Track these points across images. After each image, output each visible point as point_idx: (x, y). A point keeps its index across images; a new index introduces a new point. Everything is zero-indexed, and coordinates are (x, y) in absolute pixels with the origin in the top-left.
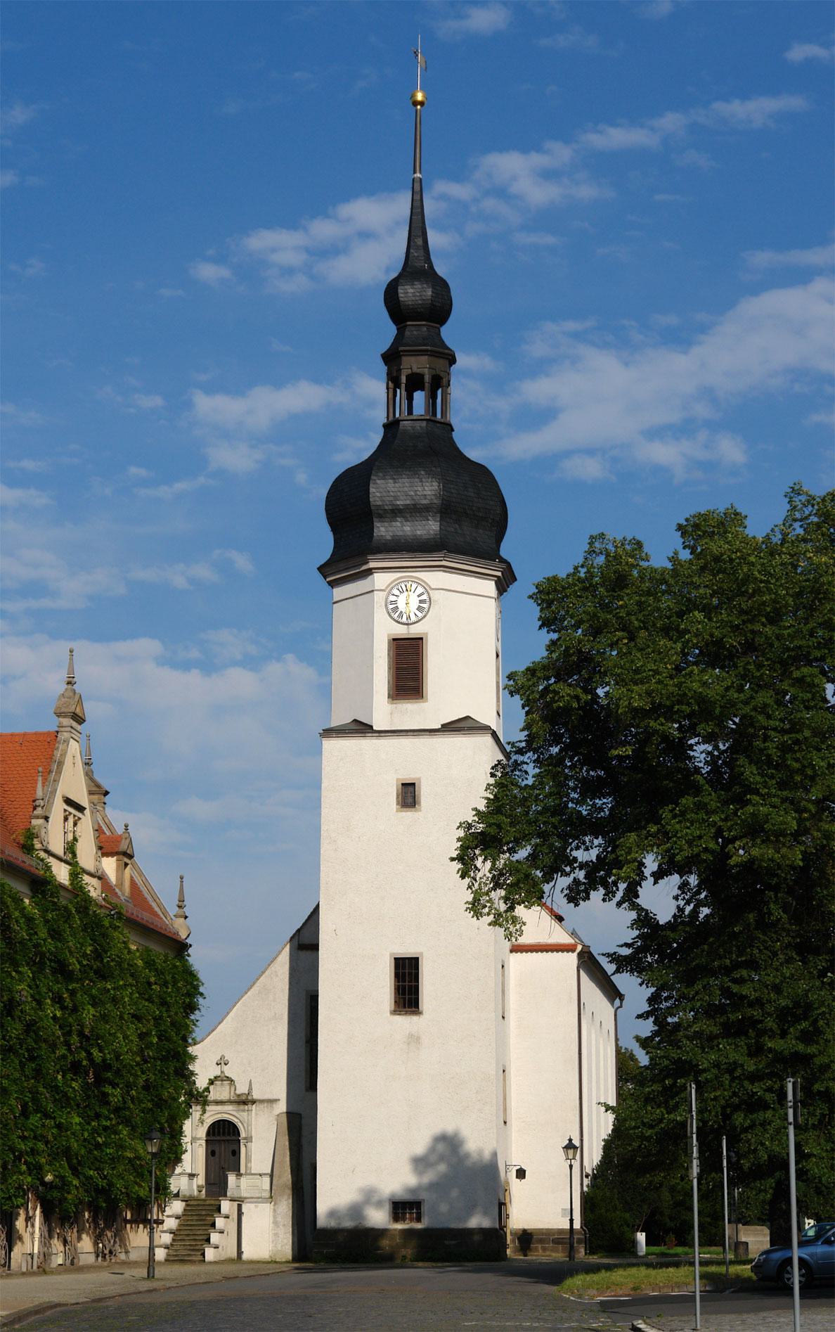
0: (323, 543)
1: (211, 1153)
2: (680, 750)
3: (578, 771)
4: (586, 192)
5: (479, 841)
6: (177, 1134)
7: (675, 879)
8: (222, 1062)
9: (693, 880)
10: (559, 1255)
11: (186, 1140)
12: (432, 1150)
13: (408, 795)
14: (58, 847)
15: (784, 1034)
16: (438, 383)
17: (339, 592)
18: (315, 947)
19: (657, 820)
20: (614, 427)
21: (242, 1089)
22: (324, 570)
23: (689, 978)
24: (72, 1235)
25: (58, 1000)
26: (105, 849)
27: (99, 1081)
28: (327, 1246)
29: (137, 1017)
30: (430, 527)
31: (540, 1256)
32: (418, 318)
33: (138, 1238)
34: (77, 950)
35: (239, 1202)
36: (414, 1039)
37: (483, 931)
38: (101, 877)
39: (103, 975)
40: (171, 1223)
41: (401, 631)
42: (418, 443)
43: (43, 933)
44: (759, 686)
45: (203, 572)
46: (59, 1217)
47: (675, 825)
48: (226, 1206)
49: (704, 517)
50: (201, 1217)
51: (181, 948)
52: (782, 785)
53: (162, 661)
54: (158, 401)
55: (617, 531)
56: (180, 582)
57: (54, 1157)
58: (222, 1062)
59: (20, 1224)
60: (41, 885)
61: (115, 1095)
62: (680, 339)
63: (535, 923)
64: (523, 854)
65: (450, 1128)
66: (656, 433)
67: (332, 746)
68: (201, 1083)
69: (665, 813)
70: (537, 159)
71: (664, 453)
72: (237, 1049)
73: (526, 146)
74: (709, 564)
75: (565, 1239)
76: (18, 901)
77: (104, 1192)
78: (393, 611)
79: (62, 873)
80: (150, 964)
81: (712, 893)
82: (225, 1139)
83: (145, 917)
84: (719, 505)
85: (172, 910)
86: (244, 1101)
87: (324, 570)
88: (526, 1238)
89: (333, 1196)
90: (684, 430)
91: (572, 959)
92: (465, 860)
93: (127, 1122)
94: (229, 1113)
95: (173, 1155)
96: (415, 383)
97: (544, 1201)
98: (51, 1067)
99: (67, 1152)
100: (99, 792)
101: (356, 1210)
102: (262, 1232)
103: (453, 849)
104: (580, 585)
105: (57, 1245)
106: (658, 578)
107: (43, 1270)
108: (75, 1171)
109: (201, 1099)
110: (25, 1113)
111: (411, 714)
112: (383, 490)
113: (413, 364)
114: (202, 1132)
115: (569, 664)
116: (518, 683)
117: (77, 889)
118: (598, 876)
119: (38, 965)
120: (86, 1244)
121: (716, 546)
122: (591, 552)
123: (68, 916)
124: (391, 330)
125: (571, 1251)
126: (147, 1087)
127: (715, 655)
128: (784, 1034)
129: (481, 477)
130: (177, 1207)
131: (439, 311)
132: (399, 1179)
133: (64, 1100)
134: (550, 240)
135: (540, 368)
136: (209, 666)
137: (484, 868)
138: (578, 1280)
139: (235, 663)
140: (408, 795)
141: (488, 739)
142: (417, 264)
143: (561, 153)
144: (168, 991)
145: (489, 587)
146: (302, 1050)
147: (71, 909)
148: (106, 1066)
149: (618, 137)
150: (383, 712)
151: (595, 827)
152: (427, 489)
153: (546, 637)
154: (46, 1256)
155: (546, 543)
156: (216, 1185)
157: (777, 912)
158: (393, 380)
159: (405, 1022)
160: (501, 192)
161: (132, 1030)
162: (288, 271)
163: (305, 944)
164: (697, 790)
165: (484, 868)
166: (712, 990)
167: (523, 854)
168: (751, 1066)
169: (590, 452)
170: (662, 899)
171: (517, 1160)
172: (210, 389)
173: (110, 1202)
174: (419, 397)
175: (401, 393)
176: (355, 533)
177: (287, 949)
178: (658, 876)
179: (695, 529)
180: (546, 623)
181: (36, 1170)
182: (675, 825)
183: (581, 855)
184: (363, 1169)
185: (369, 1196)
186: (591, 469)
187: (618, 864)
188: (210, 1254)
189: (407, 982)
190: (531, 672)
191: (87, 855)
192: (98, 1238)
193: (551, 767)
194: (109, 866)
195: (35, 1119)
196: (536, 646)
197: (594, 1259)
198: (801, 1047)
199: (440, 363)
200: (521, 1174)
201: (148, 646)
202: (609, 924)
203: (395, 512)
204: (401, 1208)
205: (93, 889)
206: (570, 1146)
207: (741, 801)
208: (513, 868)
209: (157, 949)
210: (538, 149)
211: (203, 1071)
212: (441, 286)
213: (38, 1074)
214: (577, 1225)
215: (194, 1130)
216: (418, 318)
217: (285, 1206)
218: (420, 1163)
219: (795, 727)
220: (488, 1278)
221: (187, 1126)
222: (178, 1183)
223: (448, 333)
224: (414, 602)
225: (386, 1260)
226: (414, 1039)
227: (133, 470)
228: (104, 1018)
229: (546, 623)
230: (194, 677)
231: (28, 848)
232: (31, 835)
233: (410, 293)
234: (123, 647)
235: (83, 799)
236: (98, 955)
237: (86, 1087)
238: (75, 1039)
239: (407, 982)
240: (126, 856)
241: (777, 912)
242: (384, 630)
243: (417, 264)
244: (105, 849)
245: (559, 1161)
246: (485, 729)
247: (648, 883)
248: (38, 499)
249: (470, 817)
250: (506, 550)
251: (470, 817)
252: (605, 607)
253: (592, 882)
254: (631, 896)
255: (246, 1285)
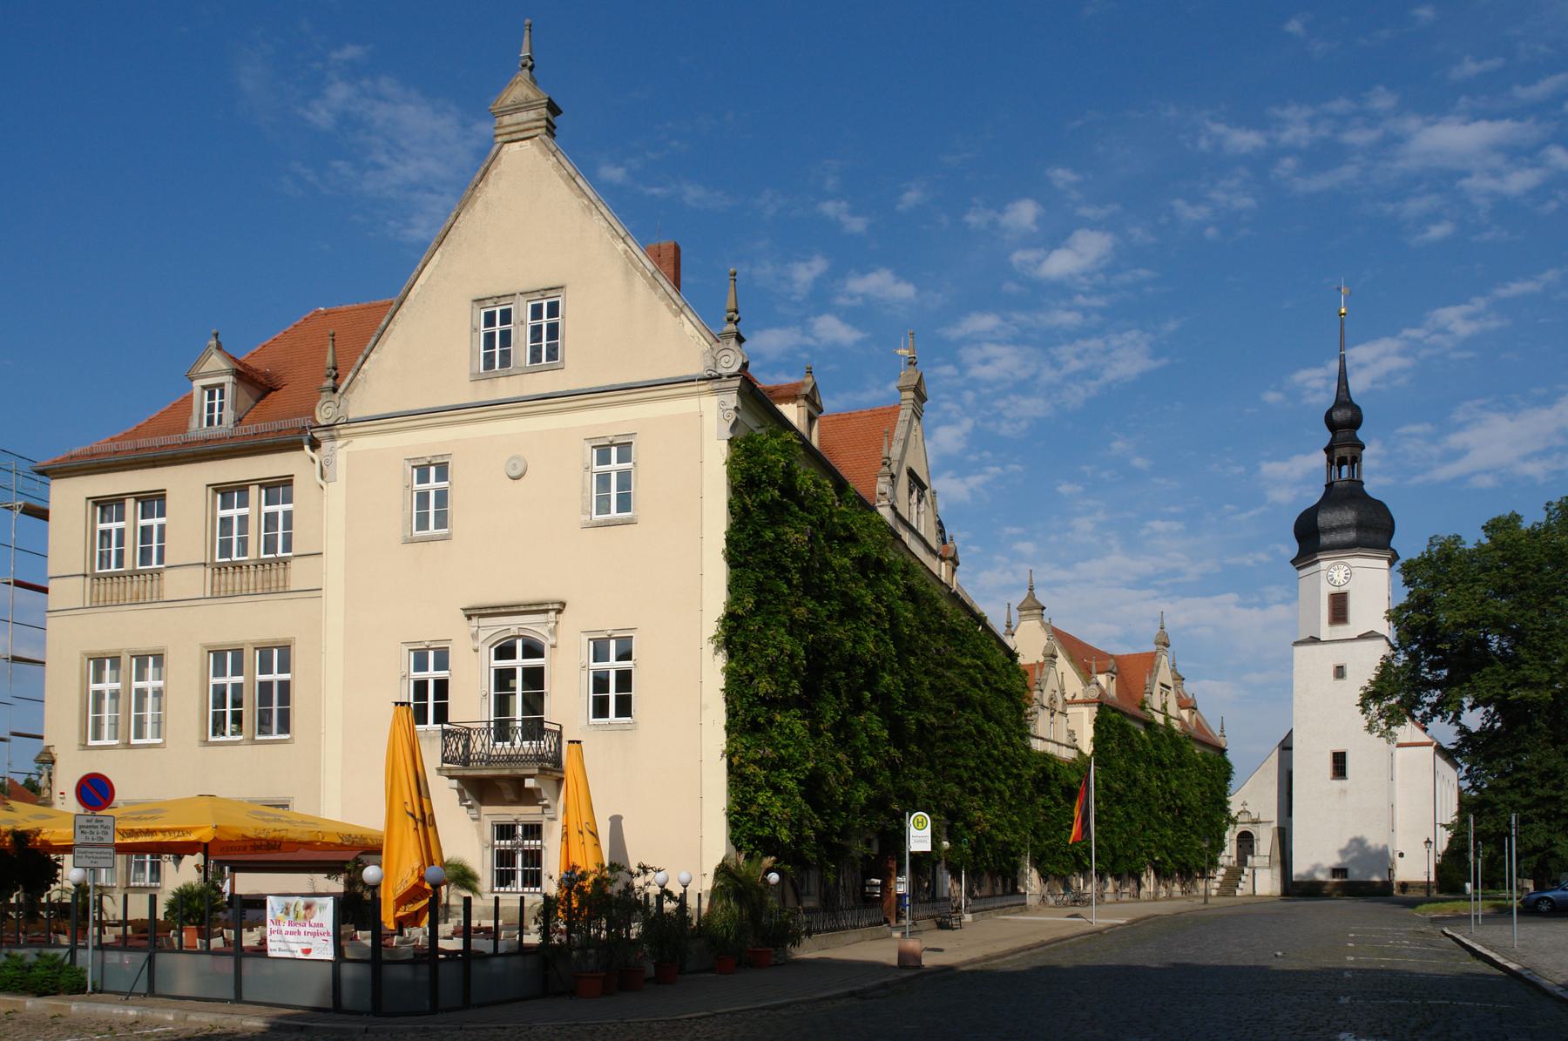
0: (1292, 549)
1: (1239, 846)
2: (1484, 643)
3: (1426, 660)
4: (1493, 324)
5: (1372, 695)
6: (1222, 838)
7: (1481, 710)
8: (1244, 804)
9: (1492, 710)
10: (1422, 894)
11: (1226, 841)
12: (1349, 846)
13: (1340, 672)
14: (1158, 706)
15: (1542, 786)
16: (1355, 460)
17: (1302, 573)
18: (1291, 749)
19: (1469, 680)
20: (1473, 467)
21: (1254, 816)
22: (1293, 562)
23: (1488, 759)
24: (1169, 884)
25: (1159, 778)
26: (1181, 706)
27: (1181, 814)
28: (1297, 889)
29: (1200, 785)
30: (1352, 535)
31: (1410, 894)
32: (1344, 427)
33: (1201, 885)
34: (1168, 754)
35: (1254, 869)
36: (1343, 792)
37: (1376, 742)
38: (1180, 719)
39: (1181, 765)
40: (1219, 878)
41: (1335, 590)
42: (1343, 491)
43: (1150, 747)
44: (1530, 607)
45: (1262, 557)
46: (1162, 875)
47: (1479, 682)
48: (1246, 870)
49: (1499, 519)
50: (1234, 876)
51: (1223, 751)
52: (1542, 658)
53: (1238, 605)
54: (1242, 469)
55: (1445, 532)
56: (1249, 562)
57: (1158, 850)
58: (1244, 804)
59: (1144, 879)
60: (1149, 725)
61: (1189, 820)
62: (1547, 401)
63: (1408, 731)
64: (1394, 701)
65: (1358, 835)
66: (1526, 458)
67: (1297, 649)
68: (1234, 814)
69: (1474, 677)
70: (1464, 309)
71: (1534, 469)
72: (1252, 797)
73: (1457, 301)
74: (1498, 545)
75: (1427, 886)
76: (1137, 733)
77: (1185, 865)
78: (1331, 581)
79: (1160, 719)
80: (1206, 759)
81: (1502, 715)
82: (1246, 840)
83: (1204, 737)
84: (1504, 511)
85: (1218, 733)
86: (1256, 822)
87: (1293, 562)
88: (1404, 886)
89: (1300, 868)
90: (1545, 454)
91: (1431, 749)
92: (1364, 705)
93: (1196, 833)
94: (1248, 827)
95: (1221, 848)
96: (1342, 462)
97: (1415, 867)
98: (1155, 809)
99: (1165, 847)
100: (1179, 679)
101: (1311, 873)
102: (1265, 882)
103: (1357, 700)
104: (1426, 561)
105: (1162, 888)
106: (1471, 555)
107: (1155, 899)
108: (1170, 856)
109: (1234, 821)
110: (1144, 829)
111: (1341, 631)
112: (1324, 519)
113: (1340, 452)
114: (1235, 837)
115: (1420, 603)
116: (1394, 616)
117: (1168, 726)
118: (1436, 709)
119: (1148, 762)
120: (1177, 887)
121: (1501, 536)
122: (1432, 544)
123: (1163, 739)
124: (1329, 435)
125: (1428, 892)
126: (1206, 816)
127: (1503, 591)
128: (1542, 786)
129: (1380, 507)
130: (1222, 871)
131: (1355, 422)
132: (1334, 860)
133: (1163, 824)
134: (1470, 354)
135: (1460, 427)
136: (1263, 605)
137: (1374, 709)
138: (1424, 907)
139: (1278, 603)
140: (1340, 672)
141: (1384, 642)
142: (1343, 398)
143: (1479, 303)
144: (1215, 770)
145: (1385, 564)
146: (1285, 796)
147: (1166, 737)
148: (1183, 807)
149: (1516, 288)
150: (1326, 631)
151: (1435, 685)
152: (1349, 516)
153: (1407, 590)
154: (1157, 893)
155: (1411, 542)
156: (1242, 861)
157: (1539, 723)
158: (1330, 461)
159: (1338, 783)
160: (1443, 331)
161: (1197, 791)
162: (1316, 391)
163: (1286, 747)
164: (1491, 663)
165: (1374, 709)
166: (1504, 763)
167: (1394, 701)
168: (1525, 802)
169: (1487, 472)
170: (1474, 719)
171: (1400, 849)
172: (1269, 460)
173: (1187, 866)
174: (1345, 468)
175: (1335, 468)
176: (1311, 540)
177: (1276, 753)
178: (1472, 708)
179: (1492, 527)
180: (1407, 583)
181: (1150, 855)
182: (1479, 682)
183: (1428, 700)
184: (1315, 854)
185: (1316, 867)
186: (1487, 482)
187: (1448, 704)
188: (1238, 892)
189: (1339, 764)
190: (1399, 609)
191: (1173, 709)
192: (1183, 885)
193: (1414, 657)
194: (1185, 714)
195: (1149, 832)
196: (1403, 598)
197: (1442, 896)
198: (1554, 793)
199: (1356, 450)
200: (1401, 855)
201: (1232, 597)
202: (1446, 732)
203: (1332, 530)
204: (1336, 872)
205: (1176, 725)
206: (1428, 841)
207: (1517, 668)
208: (1389, 708)
209: (1210, 752)
210: (1466, 302)
211: (1234, 808)
212: (1357, 410)
213: (1150, 811)
214: (1432, 879)
215: (1231, 836)
216: (1344, 427)
217: (1277, 871)
218: (1343, 852)
219: (1551, 627)
220: (1378, 905)
221: (1227, 834)
222: (1223, 860)
223: (1361, 434)
224: (1342, 575)
225: (1328, 896)
226: (1343, 792)
227: (1227, 507)
228: (1183, 785)
229: (1407, 583)
230: (1255, 611)
231: (1143, 708)
232: (1144, 702)
233: (1339, 415)
234: (1218, 599)
235: (1170, 683)
236: (1178, 756)
237: (1174, 818)
238: (1168, 796)
239: (1339, 764)
240: (1193, 708)
241: (1539, 723)
242: (1326, 590)
243: (1343, 398)
244: (1181, 706)
245: (1422, 849)
246: (1382, 636)
247: (1467, 712)
248: (1177, 526)
249: (1367, 684)
250: (1393, 545)
251: (1367, 684)
252: (1439, 572)
253: (1434, 712)
254: (1457, 717)
255: (1257, 908)
